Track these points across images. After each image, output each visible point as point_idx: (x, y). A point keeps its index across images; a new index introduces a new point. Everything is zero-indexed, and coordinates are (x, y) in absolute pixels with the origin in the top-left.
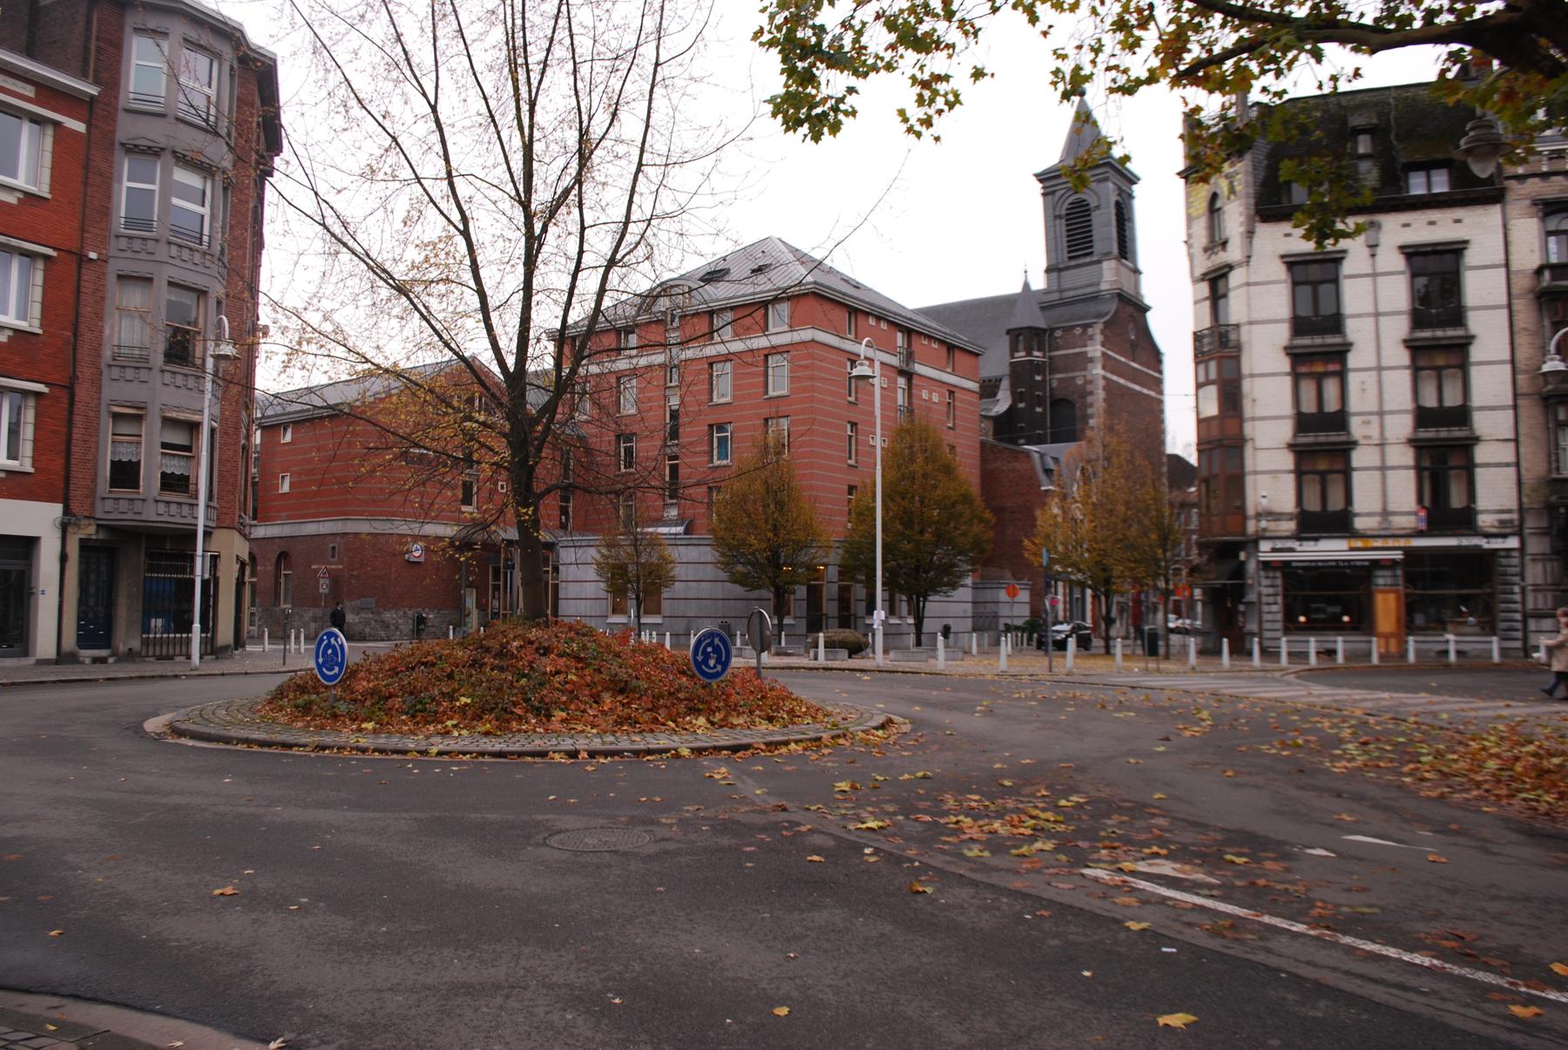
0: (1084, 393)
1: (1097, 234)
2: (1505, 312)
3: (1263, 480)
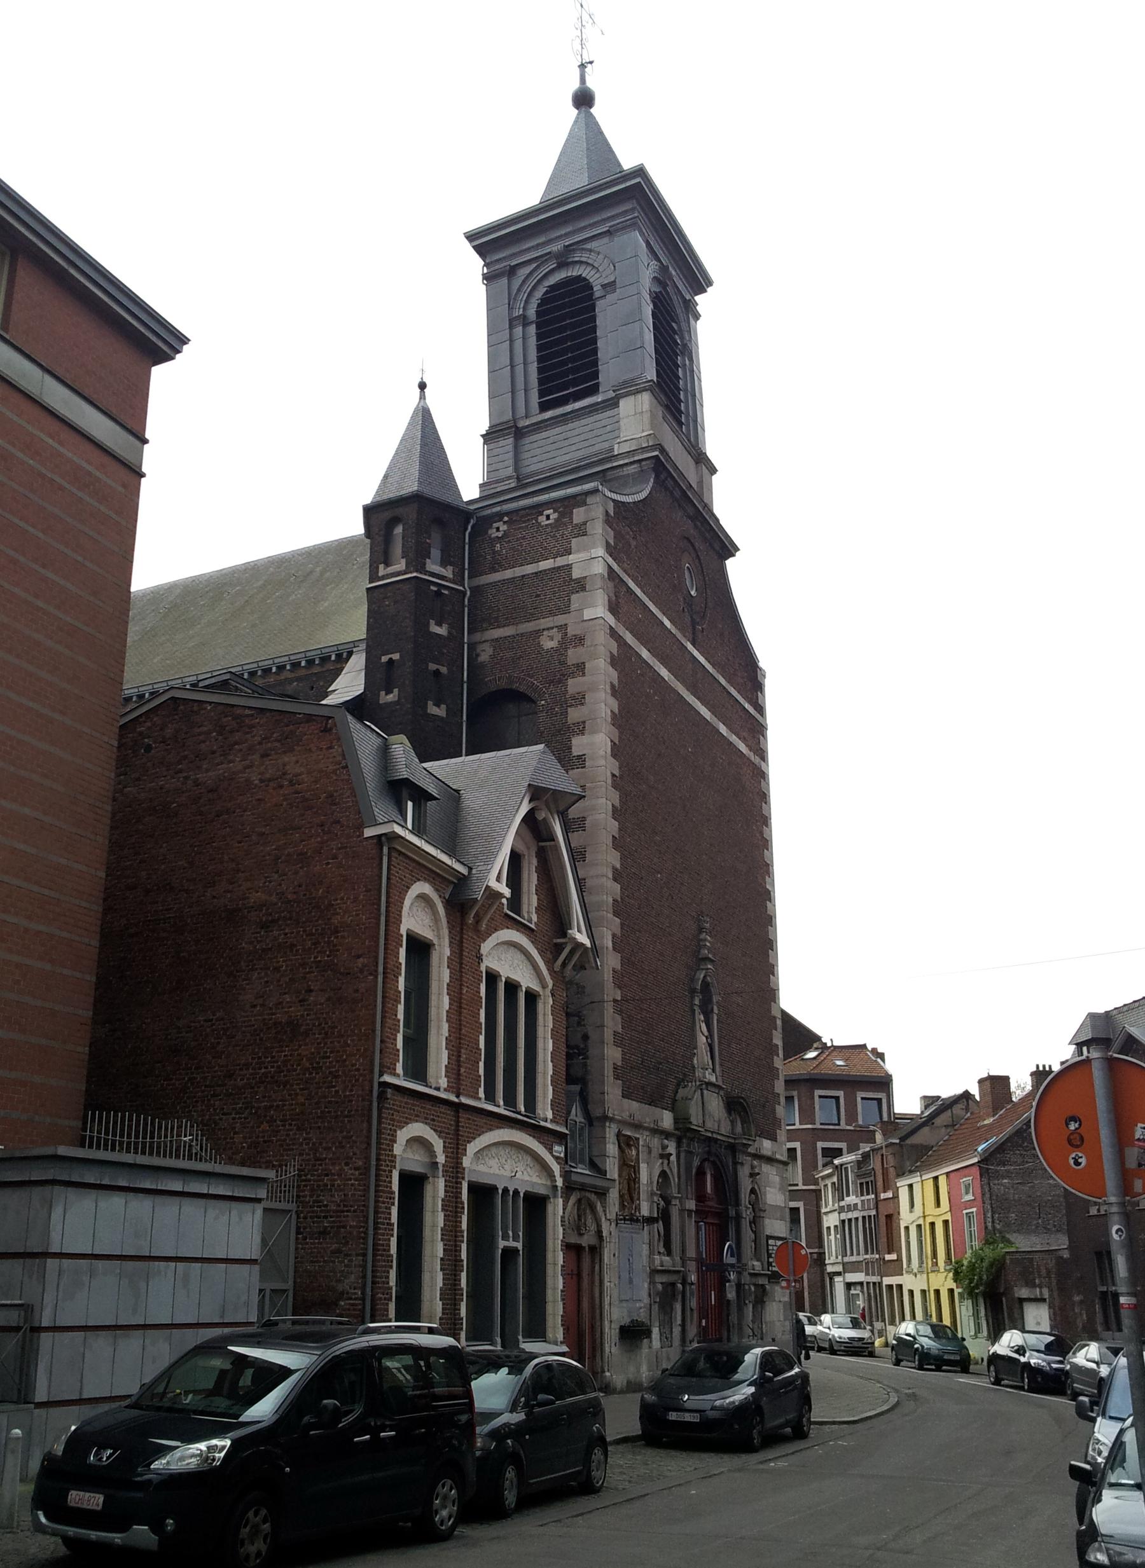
0: (561, 670)
1: (606, 347)
2: (52, 1325)
3: (176, 1209)
